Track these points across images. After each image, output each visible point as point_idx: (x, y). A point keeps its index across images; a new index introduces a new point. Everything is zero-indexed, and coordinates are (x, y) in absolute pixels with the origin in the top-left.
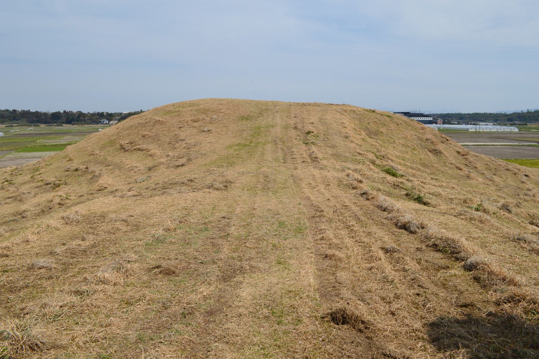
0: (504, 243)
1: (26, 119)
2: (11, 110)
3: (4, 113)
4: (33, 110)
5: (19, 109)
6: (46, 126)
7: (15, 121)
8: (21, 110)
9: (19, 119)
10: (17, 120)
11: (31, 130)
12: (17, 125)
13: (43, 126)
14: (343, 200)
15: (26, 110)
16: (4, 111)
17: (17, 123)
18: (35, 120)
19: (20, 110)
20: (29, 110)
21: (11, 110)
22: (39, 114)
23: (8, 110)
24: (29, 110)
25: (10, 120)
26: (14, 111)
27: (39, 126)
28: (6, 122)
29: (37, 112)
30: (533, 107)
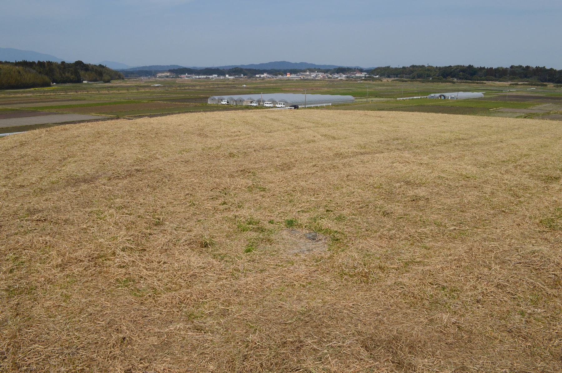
0: (124, 165)
1: (537, 77)
2: (509, 67)
3: (517, 69)
4: (495, 67)
5: (533, 65)
6: (554, 86)
7: (526, 78)
8: (535, 67)
9: (531, 77)
10: (529, 78)
11: (532, 91)
12: (526, 83)
13: (551, 85)
14: (66, 323)
15: (540, 67)
16: (517, 67)
17: (527, 81)
18: (548, 78)
19: (534, 67)
20: (537, 67)
21: (525, 67)
22: (553, 72)
23: (521, 66)
24: (544, 67)
25: (521, 77)
26: (528, 67)
27: (546, 85)
28: (516, 79)
29: (551, 69)
30: (558, 67)
